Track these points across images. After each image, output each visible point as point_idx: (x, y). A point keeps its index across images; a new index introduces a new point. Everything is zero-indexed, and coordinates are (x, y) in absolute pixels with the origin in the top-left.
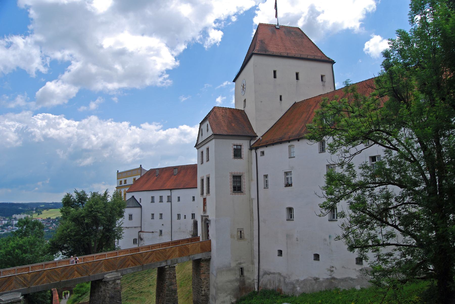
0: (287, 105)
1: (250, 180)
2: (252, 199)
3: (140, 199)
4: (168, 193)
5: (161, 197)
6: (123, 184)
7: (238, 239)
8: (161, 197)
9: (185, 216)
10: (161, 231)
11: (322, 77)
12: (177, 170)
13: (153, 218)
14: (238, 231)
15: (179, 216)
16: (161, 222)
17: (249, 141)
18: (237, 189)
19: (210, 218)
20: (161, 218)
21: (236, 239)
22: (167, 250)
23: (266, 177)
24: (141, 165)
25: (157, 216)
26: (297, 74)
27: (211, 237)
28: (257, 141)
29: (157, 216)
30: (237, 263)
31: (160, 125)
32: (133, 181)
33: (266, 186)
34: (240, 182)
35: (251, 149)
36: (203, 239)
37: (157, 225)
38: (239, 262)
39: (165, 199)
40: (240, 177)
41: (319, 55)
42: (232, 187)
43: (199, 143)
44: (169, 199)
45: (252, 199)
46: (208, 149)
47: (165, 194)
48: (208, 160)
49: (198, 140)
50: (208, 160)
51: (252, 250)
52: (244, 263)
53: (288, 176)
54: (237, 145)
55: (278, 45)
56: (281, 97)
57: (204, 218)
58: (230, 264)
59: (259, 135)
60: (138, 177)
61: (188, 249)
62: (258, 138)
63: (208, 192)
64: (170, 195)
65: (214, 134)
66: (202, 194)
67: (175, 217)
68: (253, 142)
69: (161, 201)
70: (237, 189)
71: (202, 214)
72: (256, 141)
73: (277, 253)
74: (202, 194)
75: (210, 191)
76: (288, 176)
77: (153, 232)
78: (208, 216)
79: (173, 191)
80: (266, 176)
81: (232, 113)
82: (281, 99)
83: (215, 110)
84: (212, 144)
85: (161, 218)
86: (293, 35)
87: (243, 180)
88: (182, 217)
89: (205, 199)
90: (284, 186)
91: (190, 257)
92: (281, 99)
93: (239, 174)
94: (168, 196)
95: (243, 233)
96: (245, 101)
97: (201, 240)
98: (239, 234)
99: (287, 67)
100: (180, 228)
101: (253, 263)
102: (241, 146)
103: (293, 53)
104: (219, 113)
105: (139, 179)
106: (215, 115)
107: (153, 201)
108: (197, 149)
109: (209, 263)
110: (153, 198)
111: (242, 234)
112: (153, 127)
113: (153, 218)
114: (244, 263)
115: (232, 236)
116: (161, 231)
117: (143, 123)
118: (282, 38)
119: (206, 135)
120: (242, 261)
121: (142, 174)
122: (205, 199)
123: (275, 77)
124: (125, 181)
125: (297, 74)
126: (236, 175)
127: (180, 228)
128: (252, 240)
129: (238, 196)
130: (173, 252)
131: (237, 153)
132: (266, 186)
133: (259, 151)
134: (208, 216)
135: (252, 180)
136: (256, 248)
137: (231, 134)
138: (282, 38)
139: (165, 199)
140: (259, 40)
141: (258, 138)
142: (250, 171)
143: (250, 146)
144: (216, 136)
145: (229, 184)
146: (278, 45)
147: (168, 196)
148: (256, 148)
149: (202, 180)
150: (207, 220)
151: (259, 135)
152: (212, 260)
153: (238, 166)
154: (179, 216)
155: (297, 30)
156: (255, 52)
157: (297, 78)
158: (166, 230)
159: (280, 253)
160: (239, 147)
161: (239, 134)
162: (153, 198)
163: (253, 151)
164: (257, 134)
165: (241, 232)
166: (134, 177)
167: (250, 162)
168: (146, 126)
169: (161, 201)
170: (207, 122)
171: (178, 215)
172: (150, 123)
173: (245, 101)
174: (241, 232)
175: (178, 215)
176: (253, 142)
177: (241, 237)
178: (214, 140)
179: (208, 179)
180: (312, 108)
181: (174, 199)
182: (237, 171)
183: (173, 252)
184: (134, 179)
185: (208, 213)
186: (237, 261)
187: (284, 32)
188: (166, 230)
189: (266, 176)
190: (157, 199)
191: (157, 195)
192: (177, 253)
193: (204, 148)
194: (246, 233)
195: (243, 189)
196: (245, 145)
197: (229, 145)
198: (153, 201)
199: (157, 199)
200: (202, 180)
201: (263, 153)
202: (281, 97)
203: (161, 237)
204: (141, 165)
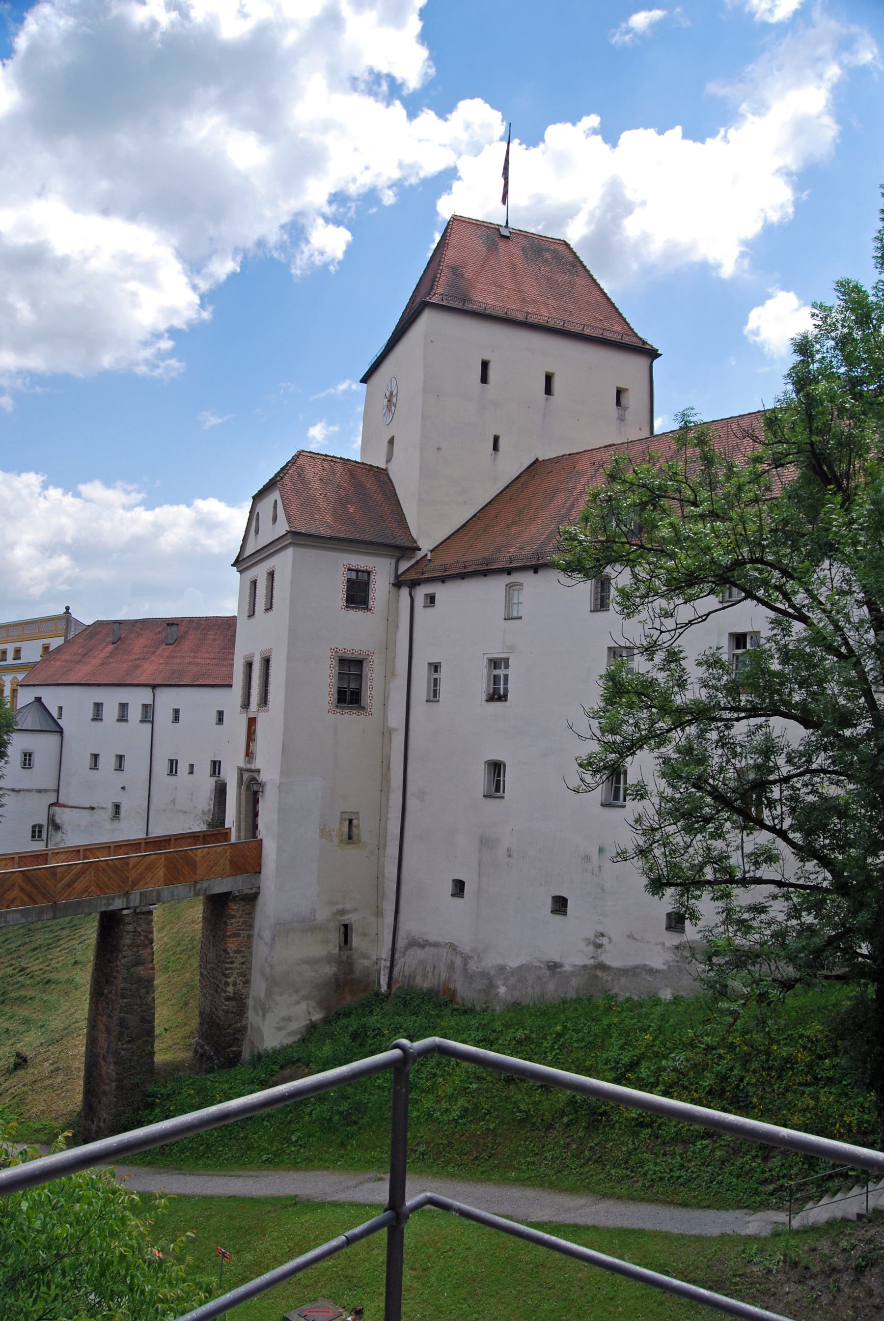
0: (511, 466)
1: (389, 674)
2: (390, 731)
3: (61, 708)
4: (144, 696)
5: (123, 707)
6: (10, 660)
7: (341, 841)
8: (123, 707)
10: (117, 807)
12: (174, 628)
13: (95, 766)
14: (342, 820)
15: (173, 765)
16: (120, 779)
17: (393, 562)
18: (349, 696)
19: (263, 777)
21: (336, 840)
23: (436, 671)
24: (67, 608)
25: (107, 762)
26: (549, 378)
28: (417, 562)
29: (107, 762)
30: (335, 909)
32: (40, 651)
33: (434, 695)
35: (398, 584)
36: (239, 838)
37: (105, 787)
38: (340, 907)
41: (617, 328)
42: (334, 691)
43: (247, 553)
44: (148, 714)
45: (390, 731)
46: (271, 574)
47: (137, 698)
48: (269, 608)
49: (243, 547)
50: (269, 608)
51: (379, 877)
52: (355, 910)
55: (502, 287)
56: (496, 439)
57: (246, 776)
58: (314, 911)
60: (56, 643)
61: (192, 865)
62: (419, 555)
66: (246, 705)
67: (162, 767)
68: (404, 566)
69: (123, 717)
70: (349, 696)
71: (242, 765)
72: (413, 561)
73: (449, 888)
74: (246, 705)
75: (271, 697)
77: (92, 808)
78: (258, 771)
79: (159, 691)
82: (496, 447)
83: (299, 461)
84: (284, 562)
86: (546, 261)
88: (183, 768)
89: (252, 722)
90: (484, 697)
92: (496, 447)
93: (356, 656)
94: (145, 707)
95: (358, 827)
96: (391, 441)
97: (233, 839)
99: (522, 356)
100: (173, 801)
102: (369, 573)
103: (543, 316)
104: (311, 471)
105: (59, 649)
106: (300, 475)
107: (98, 717)
108: (241, 572)
109: (253, 907)
110: (98, 706)
111: (355, 830)
112: (114, 496)
113: (95, 766)
114: (355, 910)
115: (324, 833)
118: (513, 266)
119: (269, 532)
120: (348, 906)
121: (71, 635)
122: (252, 722)
124: (18, 652)
125: (549, 378)
126: (349, 656)
127: (173, 801)
128: (381, 847)
129: (349, 719)
131: (357, 594)
133: (421, 592)
134: (258, 771)
138: (513, 266)
139: (135, 713)
140: (448, 267)
141: (419, 555)
142: (389, 648)
143: (397, 576)
144: (297, 538)
146: (502, 287)
147: (145, 707)
148: (413, 584)
149: (249, 665)
151: (426, 545)
152: (261, 899)
153: (357, 632)
154: (173, 765)
155: (561, 248)
157: (548, 391)
158: (133, 804)
159: (459, 887)
162: (98, 706)
163: (405, 591)
164: (420, 544)
165: (351, 821)
166: (46, 641)
167: (391, 623)
168: (94, 490)
169: (123, 717)
170: (276, 495)
171: (171, 761)
172: (108, 484)
173: (391, 441)
174: (351, 821)
175: (171, 761)
176: (404, 566)
177: (350, 838)
178: (290, 551)
179: (267, 662)
181: (163, 715)
182: (352, 646)
184: (46, 648)
185: (257, 764)
187: (524, 249)
188: (133, 804)
190: (111, 712)
191: (111, 699)
193: (260, 572)
194: (366, 828)
195: (366, 699)
196: (382, 571)
197: (335, 568)
198: (98, 717)
199: (111, 712)
200: (249, 665)
201: (431, 600)
202: (496, 439)
203: (116, 822)
204: (67, 608)
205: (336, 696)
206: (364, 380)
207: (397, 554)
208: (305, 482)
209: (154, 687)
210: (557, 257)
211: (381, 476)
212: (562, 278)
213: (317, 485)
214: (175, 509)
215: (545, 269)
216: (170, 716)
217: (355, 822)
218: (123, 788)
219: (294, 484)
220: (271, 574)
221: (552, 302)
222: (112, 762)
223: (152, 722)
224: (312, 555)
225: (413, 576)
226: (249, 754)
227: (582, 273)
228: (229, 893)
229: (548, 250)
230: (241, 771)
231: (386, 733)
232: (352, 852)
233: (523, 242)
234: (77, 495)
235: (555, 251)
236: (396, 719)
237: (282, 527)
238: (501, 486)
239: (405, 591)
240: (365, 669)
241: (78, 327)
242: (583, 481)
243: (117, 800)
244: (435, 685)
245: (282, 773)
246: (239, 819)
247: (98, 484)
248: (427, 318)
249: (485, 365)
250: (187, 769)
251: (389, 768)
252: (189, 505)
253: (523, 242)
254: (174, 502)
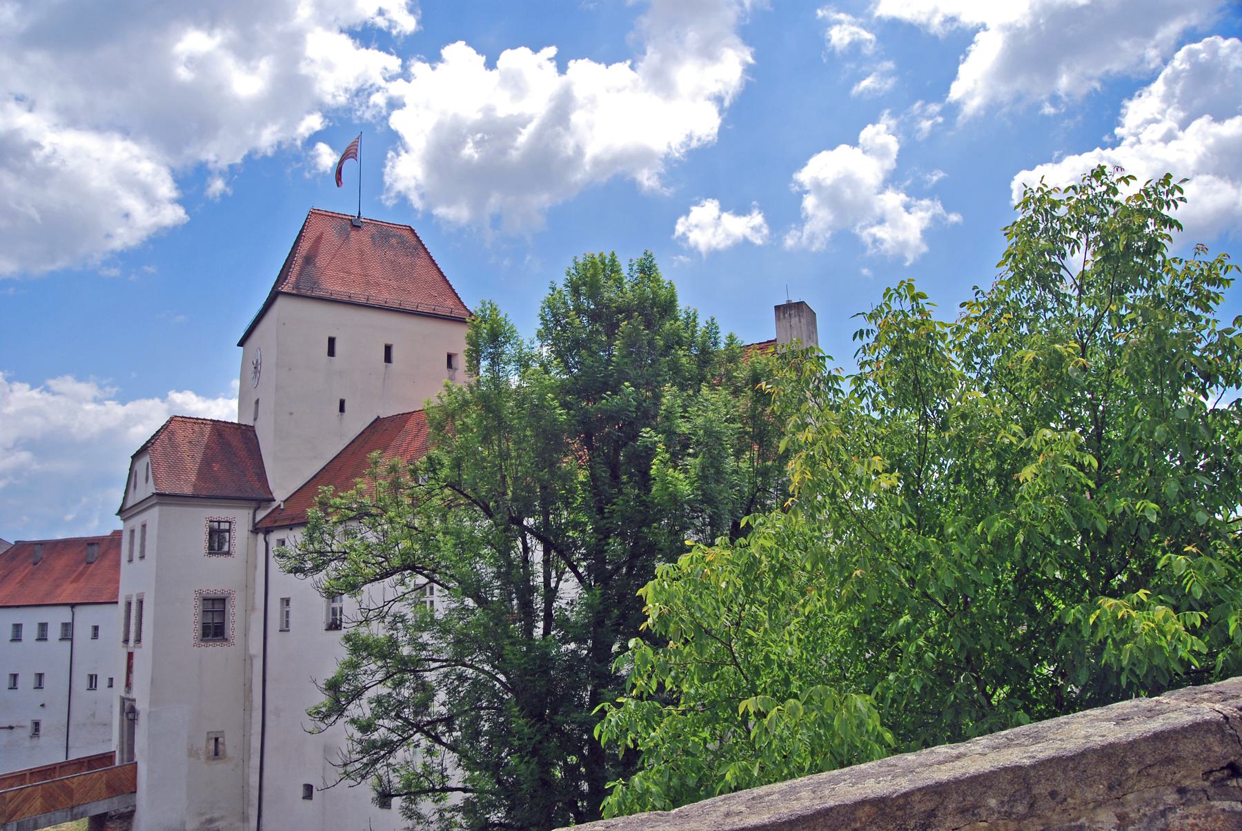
0: (355, 424)
1: (249, 609)
2: (251, 658)
4: (64, 615)
5: (43, 627)
7: (208, 758)
8: (43, 627)
9: (111, 680)
10: (37, 725)
11: (450, 357)
12: (95, 548)
13: (14, 686)
14: (208, 739)
15: (93, 679)
16: (40, 696)
17: (251, 512)
18: (214, 631)
19: (138, 706)
20: (39, 686)
21: (203, 757)
22: (9, 796)
23: (288, 604)
25: (26, 681)
26: (388, 349)
27: (138, 757)
28: (273, 511)
29: (26, 681)
30: (203, 819)
31: (113, 386)
33: (285, 629)
34: (223, 612)
35: (256, 530)
36: (122, 760)
38: (208, 817)
39: (54, 632)
40: (223, 600)
41: (450, 303)
42: (199, 627)
43: (129, 505)
44: (68, 632)
45: (251, 658)
46: (144, 526)
47: (56, 618)
48: (142, 557)
49: (125, 499)
50: (142, 557)
51: (245, 784)
52: (222, 818)
53: (334, 605)
54: (219, 522)
55: (349, 273)
56: (342, 403)
57: (127, 704)
58: (183, 823)
59: (280, 496)
61: (69, 792)
62: (275, 505)
63: (138, 640)
64: (69, 620)
65: (158, 494)
66: (126, 641)
67: (81, 683)
68: (261, 515)
69: (42, 637)
70: (214, 631)
71: (123, 695)
72: (270, 510)
73: (301, 792)
74: (126, 641)
75: (143, 635)
76: (334, 605)
77: (11, 728)
78: (134, 700)
79: (78, 610)
80: (286, 601)
81: (220, 435)
82: (342, 409)
83: (171, 427)
84: (152, 516)
85: (39, 686)
86: (392, 246)
87: (229, 609)
89: (130, 655)
90: (324, 627)
91: (75, 811)
92: (342, 409)
93: (219, 595)
94: (65, 625)
95: (223, 744)
96: (257, 402)
97: (117, 763)
98: (212, 747)
99: (363, 333)
100: (93, 715)
101: (245, 818)
106: (170, 439)
107: (17, 638)
108: (125, 520)
109: (130, 824)
110: (18, 627)
111: (220, 747)
112: (86, 389)
114: (222, 818)
115: (192, 753)
116: (37, 725)
117: (54, 377)
118: (362, 252)
119: (145, 489)
120: (216, 815)
122: (130, 655)
123: (331, 352)
126: (212, 595)
127: (93, 715)
128: (245, 759)
129: (214, 650)
130: (25, 800)
131: (217, 540)
132: (285, 629)
133: (274, 537)
134: (134, 700)
135: (253, 609)
136: (254, 779)
137: (204, 493)
138: (362, 252)
139: (54, 632)
141: (275, 505)
142: (248, 586)
143: (255, 525)
144: (162, 498)
145: (191, 618)
146: (349, 273)
147: (65, 625)
148: (267, 531)
149: (129, 604)
150: (133, 710)
151: (280, 496)
152: (137, 816)
153: (219, 575)
154: (93, 679)
155: (406, 233)
156: (285, 288)
157: (388, 359)
158: (52, 720)
159: (309, 791)
160: (224, 526)
161: (226, 493)
162: (18, 627)
163: (261, 536)
164: (275, 495)
165: (216, 740)
167: (250, 563)
168: (67, 384)
169: (42, 637)
170: (146, 459)
171: (91, 676)
172: (80, 378)
173: (257, 402)
174: (216, 740)
175: (91, 676)
176: (261, 515)
177: (216, 754)
178: (156, 510)
179: (141, 603)
180: (409, 439)
181: (82, 632)
182: (214, 587)
183: (25, 800)
185: (135, 694)
186: (202, 814)
187: (372, 237)
188: (52, 720)
189: (286, 601)
190: (30, 632)
191: (30, 620)
192: (38, 803)
193: (136, 523)
194: (230, 745)
196: (240, 519)
197: (199, 519)
198: (17, 638)
199: (30, 632)
200: (129, 604)
203: (35, 740)
205: (201, 632)
206: (241, 344)
207: (254, 504)
208: (174, 446)
209: (73, 606)
210: (402, 242)
211: (251, 429)
212: (403, 261)
213: (185, 448)
214: (150, 403)
215: (390, 254)
216: (90, 632)
217: (220, 740)
218: (43, 705)
219: (164, 448)
220: (144, 526)
221: (394, 283)
222: (32, 681)
223: (72, 640)
224: (175, 511)
225: (267, 524)
226: (128, 685)
227: (423, 254)
228: (106, 814)
229: (394, 236)
230: (123, 700)
231: (248, 659)
232: (219, 766)
233: (373, 230)
234: (47, 389)
235: (401, 236)
236: (256, 647)
237: (151, 489)
238: (347, 442)
239: (261, 536)
240: (228, 606)
241: (62, 227)
242: (409, 439)
243: (36, 718)
244: (287, 616)
245: (151, 703)
246: (122, 743)
247: (69, 378)
248: (281, 303)
249: (332, 341)
250: (106, 683)
251: (251, 691)
252: (164, 398)
253: (373, 230)
254: (150, 396)
